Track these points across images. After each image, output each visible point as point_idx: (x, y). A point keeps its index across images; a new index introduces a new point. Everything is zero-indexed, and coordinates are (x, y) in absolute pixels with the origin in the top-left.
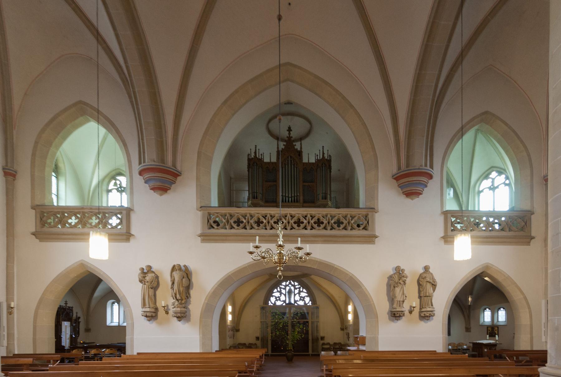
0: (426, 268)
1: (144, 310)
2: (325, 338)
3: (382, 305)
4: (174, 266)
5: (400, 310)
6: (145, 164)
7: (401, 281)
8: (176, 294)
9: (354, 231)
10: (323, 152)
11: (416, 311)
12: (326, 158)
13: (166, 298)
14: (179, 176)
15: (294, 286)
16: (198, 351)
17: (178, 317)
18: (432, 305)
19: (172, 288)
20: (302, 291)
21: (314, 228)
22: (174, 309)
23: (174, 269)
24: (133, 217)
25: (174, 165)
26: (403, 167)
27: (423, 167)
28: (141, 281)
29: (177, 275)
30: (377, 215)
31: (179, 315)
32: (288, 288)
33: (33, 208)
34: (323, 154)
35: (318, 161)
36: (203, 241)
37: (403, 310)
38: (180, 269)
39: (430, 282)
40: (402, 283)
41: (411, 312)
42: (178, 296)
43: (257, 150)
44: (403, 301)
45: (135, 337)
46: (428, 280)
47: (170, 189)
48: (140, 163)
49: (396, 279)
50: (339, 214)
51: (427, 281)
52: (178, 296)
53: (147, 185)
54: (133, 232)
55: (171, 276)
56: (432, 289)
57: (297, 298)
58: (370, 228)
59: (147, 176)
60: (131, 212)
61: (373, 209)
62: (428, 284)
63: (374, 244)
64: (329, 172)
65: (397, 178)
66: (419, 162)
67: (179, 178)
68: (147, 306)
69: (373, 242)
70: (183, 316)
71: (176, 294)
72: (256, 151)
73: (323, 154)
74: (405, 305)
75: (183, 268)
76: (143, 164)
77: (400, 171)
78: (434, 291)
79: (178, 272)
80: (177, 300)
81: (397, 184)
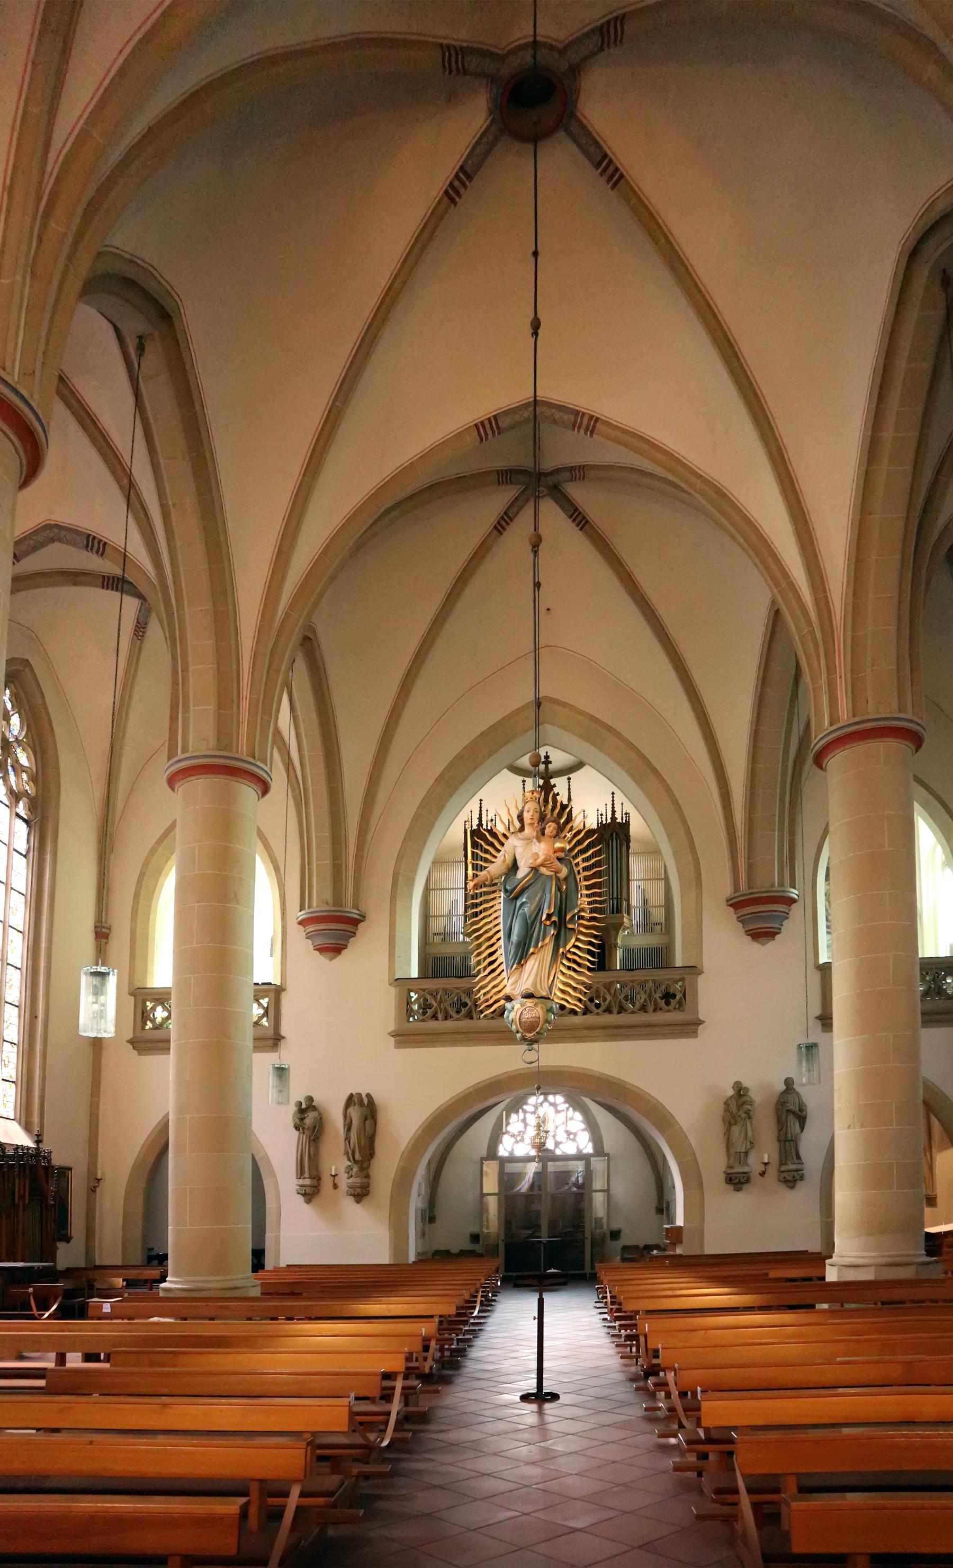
0: (789, 1082)
1: (301, 1182)
2: (622, 1235)
3: (713, 1163)
4: (351, 1095)
5: (741, 1170)
6: (311, 910)
7: (741, 1113)
8: (353, 1152)
9: (659, 1013)
10: (613, 807)
11: (772, 1172)
12: (619, 820)
13: (336, 1162)
14: (360, 921)
15: (554, 1105)
16: (387, 1262)
17: (354, 1195)
18: (799, 1157)
19: (348, 1139)
20: (572, 1119)
21: (591, 1012)
22: (351, 1180)
23: (351, 1100)
24: (285, 1000)
25: (356, 906)
26: (743, 885)
27: (776, 887)
28: (297, 1128)
29: (355, 1113)
30: (701, 978)
31: (359, 1191)
32: (541, 1111)
33: (131, 994)
34: (613, 812)
35: (602, 827)
36: (399, 1045)
37: (746, 1169)
38: (361, 1103)
39: (794, 1113)
40: (744, 1116)
41: (763, 1174)
42: (357, 1156)
43: (484, 813)
44: (746, 1153)
45: (282, 1234)
46: (791, 1107)
47: (345, 947)
48: (171, 754)
49: (738, 1105)
50: (632, 981)
51: (788, 1111)
52: (357, 1156)
53: (309, 942)
54: (283, 1033)
55: (345, 1115)
56: (797, 1124)
57: (561, 1136)
58: (687, 1006)
59: (311, 928)
60: (283, 994)
61: (694, 970)
62: (791, 1117)
63: (696, 1037)
64: (624, 848)
65: (736, 904)
66: (770, 877)
67: (361, 925)
68: (307, 1175)
69: (693, 1034)
70: (361, 1194)
71: (353, 1152)
72: (480, 814)
73: (613, 812)
74: (751, 1160)
75: (366, 1101)
76: (307, 910)
77: (737, 894)
78: (802, 1128)
79: (357, 1107)
80: (355, 1162)
81: (735, 917)
